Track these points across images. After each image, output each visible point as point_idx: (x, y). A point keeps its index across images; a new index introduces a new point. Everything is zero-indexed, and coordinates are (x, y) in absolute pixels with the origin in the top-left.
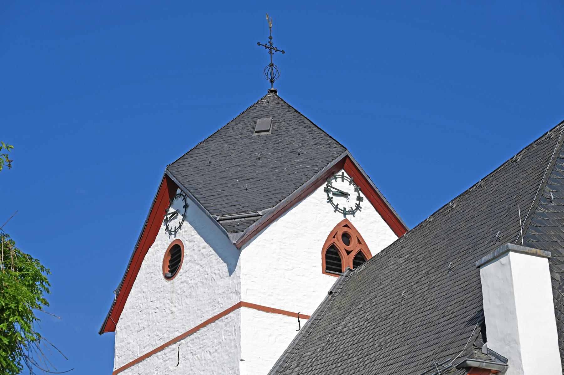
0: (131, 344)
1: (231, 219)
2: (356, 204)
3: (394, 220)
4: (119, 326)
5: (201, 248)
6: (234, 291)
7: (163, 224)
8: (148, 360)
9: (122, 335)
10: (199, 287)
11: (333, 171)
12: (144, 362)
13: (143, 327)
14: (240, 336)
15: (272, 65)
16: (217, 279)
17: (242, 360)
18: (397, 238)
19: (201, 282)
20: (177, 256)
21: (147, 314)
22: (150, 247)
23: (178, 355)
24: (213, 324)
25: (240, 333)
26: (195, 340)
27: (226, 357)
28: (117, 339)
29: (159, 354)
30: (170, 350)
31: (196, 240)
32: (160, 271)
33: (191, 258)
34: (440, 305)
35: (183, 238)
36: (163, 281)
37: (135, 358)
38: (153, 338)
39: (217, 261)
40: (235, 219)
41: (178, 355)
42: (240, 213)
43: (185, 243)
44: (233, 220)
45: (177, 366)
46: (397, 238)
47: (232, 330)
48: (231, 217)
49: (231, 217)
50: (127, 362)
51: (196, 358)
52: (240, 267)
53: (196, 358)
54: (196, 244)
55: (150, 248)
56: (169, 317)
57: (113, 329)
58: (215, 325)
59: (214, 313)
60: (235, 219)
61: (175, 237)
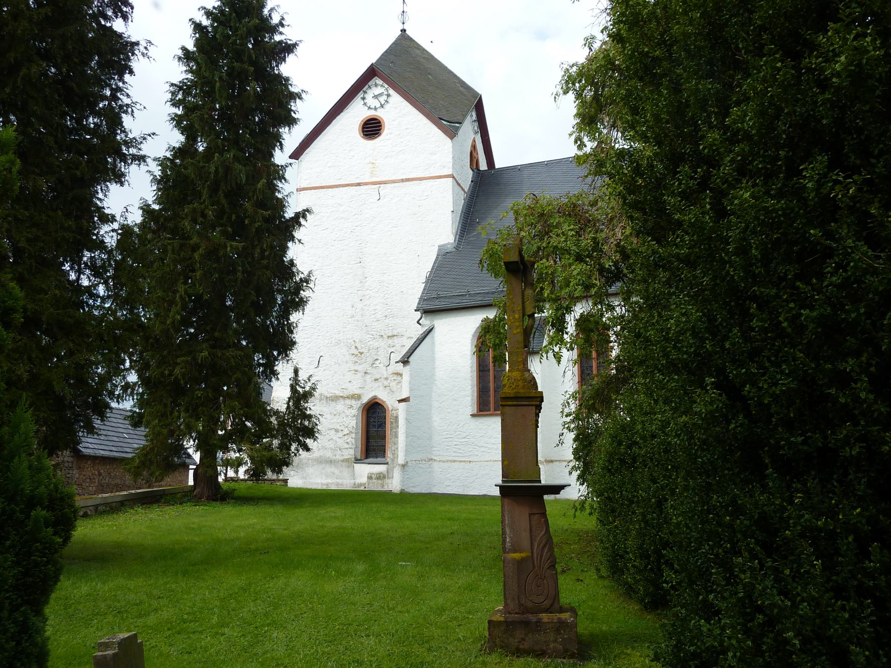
18: (487, 169)
46: (487, 169)
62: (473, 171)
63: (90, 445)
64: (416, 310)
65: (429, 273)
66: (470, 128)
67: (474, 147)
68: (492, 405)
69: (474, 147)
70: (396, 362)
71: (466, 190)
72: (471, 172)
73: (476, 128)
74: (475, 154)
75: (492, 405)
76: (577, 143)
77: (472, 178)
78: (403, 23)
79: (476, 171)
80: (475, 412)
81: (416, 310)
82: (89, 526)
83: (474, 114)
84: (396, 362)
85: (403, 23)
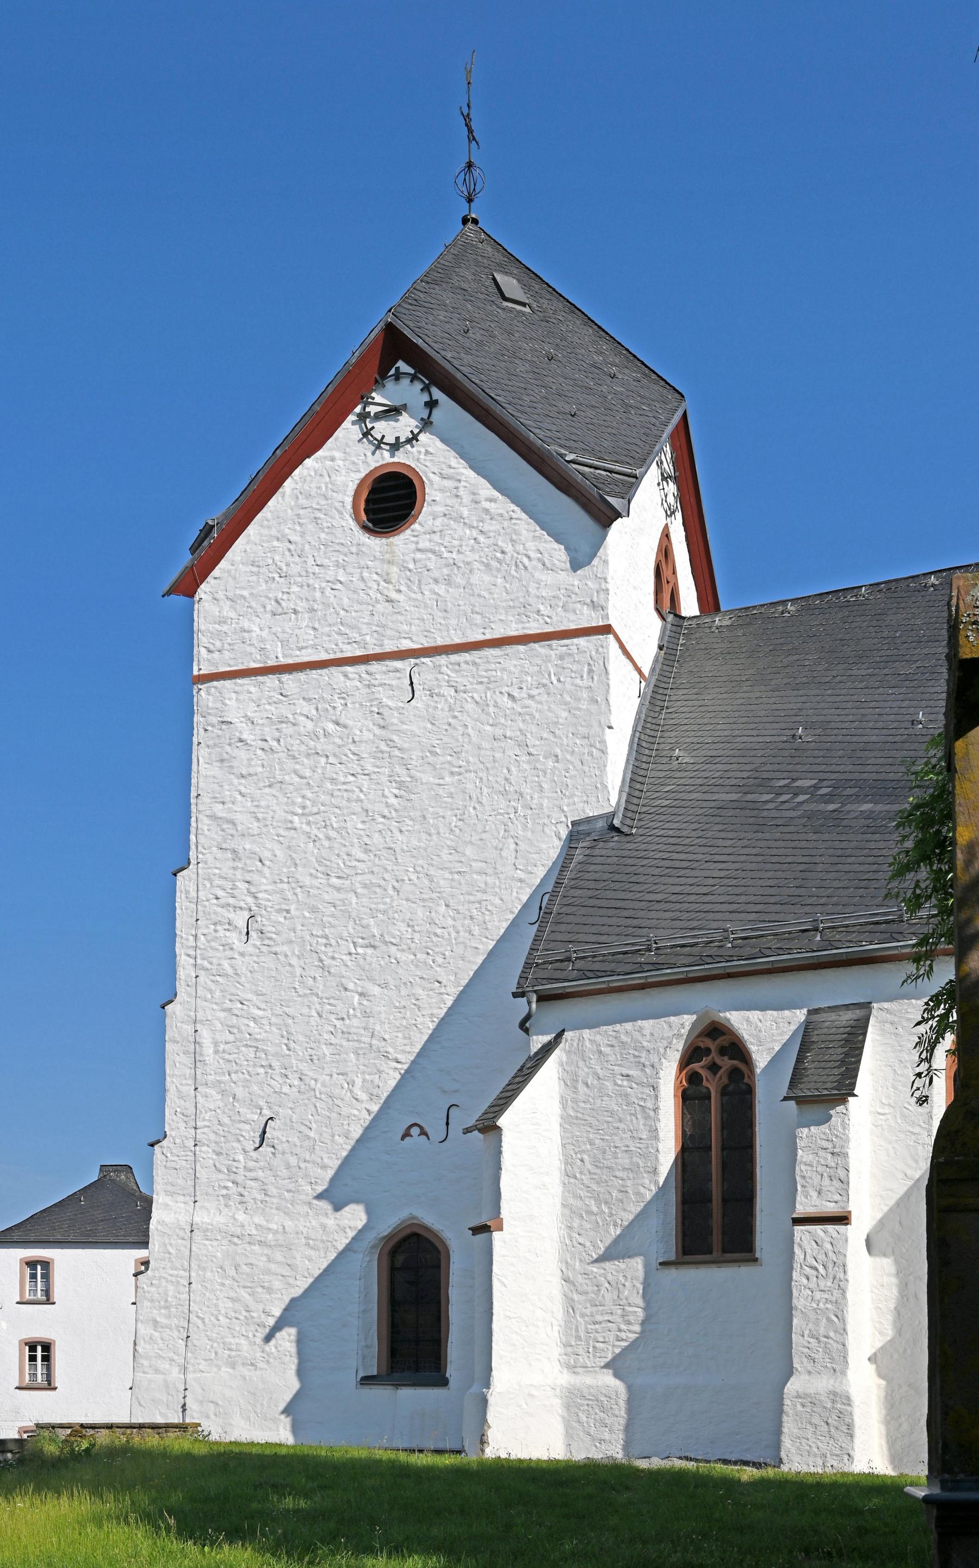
0: (254, 634)
1: (590, 467)
2: (412, 432)
3: (702, 548)
4: (204, 591)
5: (483, 499)
6: (588, 601)
7: (352, 418)
8: (314, 674)
9: (218, 609)
10: (476, 571)
11: (635, 383)
12: (302, 676)
13: (295, 610)
14: (608, 685)
15: (470, 165)
16: (535, 568)
17: (610, 727)
18: (698, 613)
19: (483, 562)
20: (386, 495)
21: (305, 587)
22: (309, 457)
23: (412, 684)
24: (521, 648)
25: (608, 679)
26: (464, 666)
27: (565, 714)
28: (202, 615)
29: (349, 669)
30: (384, 668)
31: (464, 479)
32: (345, 513)
33: (448, 510)
34: (652, 967)
35: (419, 465)
36: (356, 533)
37: (269, 662)
38: (329, 636)
39: (532, 534)
40: (596, 468)
41: (412, 684)
42: (616, 462)
43: (427, 477)
44: (592, 470)
45: (409, 702)
46: (698, 613)
47: (583, 670)
48: (630, 471)
49: (614, 467)
50: (240, 665)
51: (469, 699)
52: (606, 562)
53: (469, 699)
54: (465, 487)
55: (307, 460)
56: (379, 606)
57: (191, 593)
58: (526, 651)
59: (523, 628)
60: (596, 468)
61: (392, 456)
62: (663, 618)
63: (695, 1017)
64: (515, 995)
65: (546, 897)
66: (657, 495)
67: (666, 535)
68: (716, 1238)
69: (665, 552)
70: (467, 1131)
71: (646, 671)
72: (657, 623)
73: (671, 500)
74: (666, 573)
75: (716, 1238)
76: (160, 1528)
77: (661, 638)
78: (470, 200)
79: (670, 618)
80: (672, 1257)
81: (515, 995)
82: (961, 809)
83: (667, 454)
84: (467, 1131)
85: (470, 200)
